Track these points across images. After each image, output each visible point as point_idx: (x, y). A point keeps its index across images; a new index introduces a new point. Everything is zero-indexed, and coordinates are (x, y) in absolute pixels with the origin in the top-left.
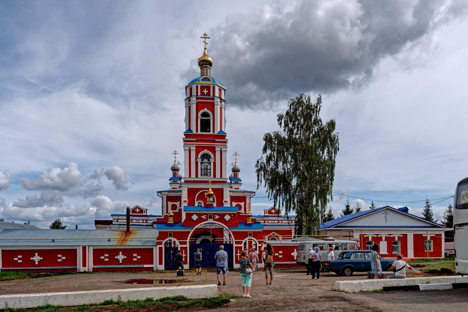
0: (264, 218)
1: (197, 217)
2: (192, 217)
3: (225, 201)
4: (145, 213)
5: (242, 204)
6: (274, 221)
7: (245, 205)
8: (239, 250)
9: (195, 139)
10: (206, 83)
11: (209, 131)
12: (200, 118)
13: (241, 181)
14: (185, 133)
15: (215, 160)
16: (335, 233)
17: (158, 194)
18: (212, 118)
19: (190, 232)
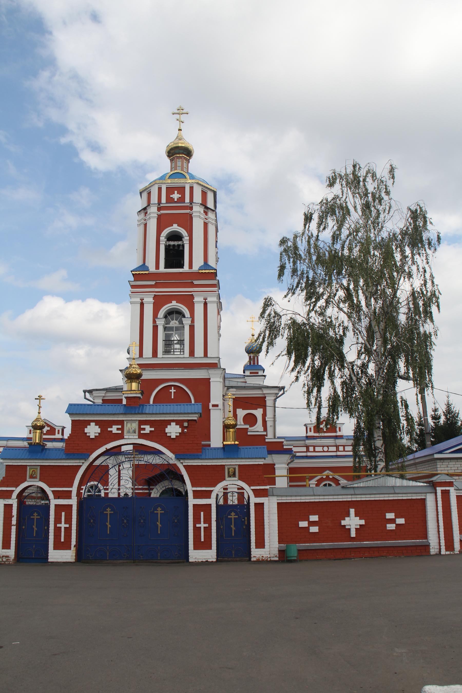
0: (305, 440)
1: (99, 430)
2: (86, 430)
3: (213, 406)
4: (58, 433)
5: (258, 413)
6: (328, 446)
7: (264, 415)
8: (202, 513)
9: (153, 283)
10: (178, 182)
11: (182, 266)
12: (164, 243)
13: (264, 370)
14: (133, 272)
15: (193, 321)
16: (455, 466)
17: (85, 395)
18: (188, 242)
19: (81, 466)
